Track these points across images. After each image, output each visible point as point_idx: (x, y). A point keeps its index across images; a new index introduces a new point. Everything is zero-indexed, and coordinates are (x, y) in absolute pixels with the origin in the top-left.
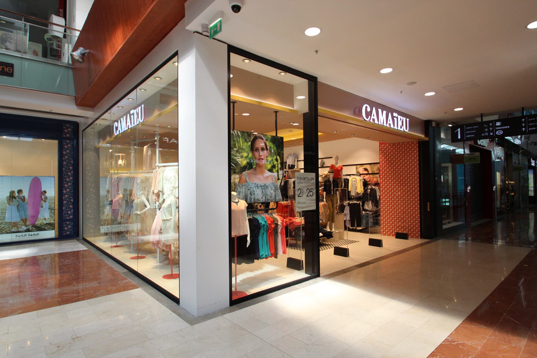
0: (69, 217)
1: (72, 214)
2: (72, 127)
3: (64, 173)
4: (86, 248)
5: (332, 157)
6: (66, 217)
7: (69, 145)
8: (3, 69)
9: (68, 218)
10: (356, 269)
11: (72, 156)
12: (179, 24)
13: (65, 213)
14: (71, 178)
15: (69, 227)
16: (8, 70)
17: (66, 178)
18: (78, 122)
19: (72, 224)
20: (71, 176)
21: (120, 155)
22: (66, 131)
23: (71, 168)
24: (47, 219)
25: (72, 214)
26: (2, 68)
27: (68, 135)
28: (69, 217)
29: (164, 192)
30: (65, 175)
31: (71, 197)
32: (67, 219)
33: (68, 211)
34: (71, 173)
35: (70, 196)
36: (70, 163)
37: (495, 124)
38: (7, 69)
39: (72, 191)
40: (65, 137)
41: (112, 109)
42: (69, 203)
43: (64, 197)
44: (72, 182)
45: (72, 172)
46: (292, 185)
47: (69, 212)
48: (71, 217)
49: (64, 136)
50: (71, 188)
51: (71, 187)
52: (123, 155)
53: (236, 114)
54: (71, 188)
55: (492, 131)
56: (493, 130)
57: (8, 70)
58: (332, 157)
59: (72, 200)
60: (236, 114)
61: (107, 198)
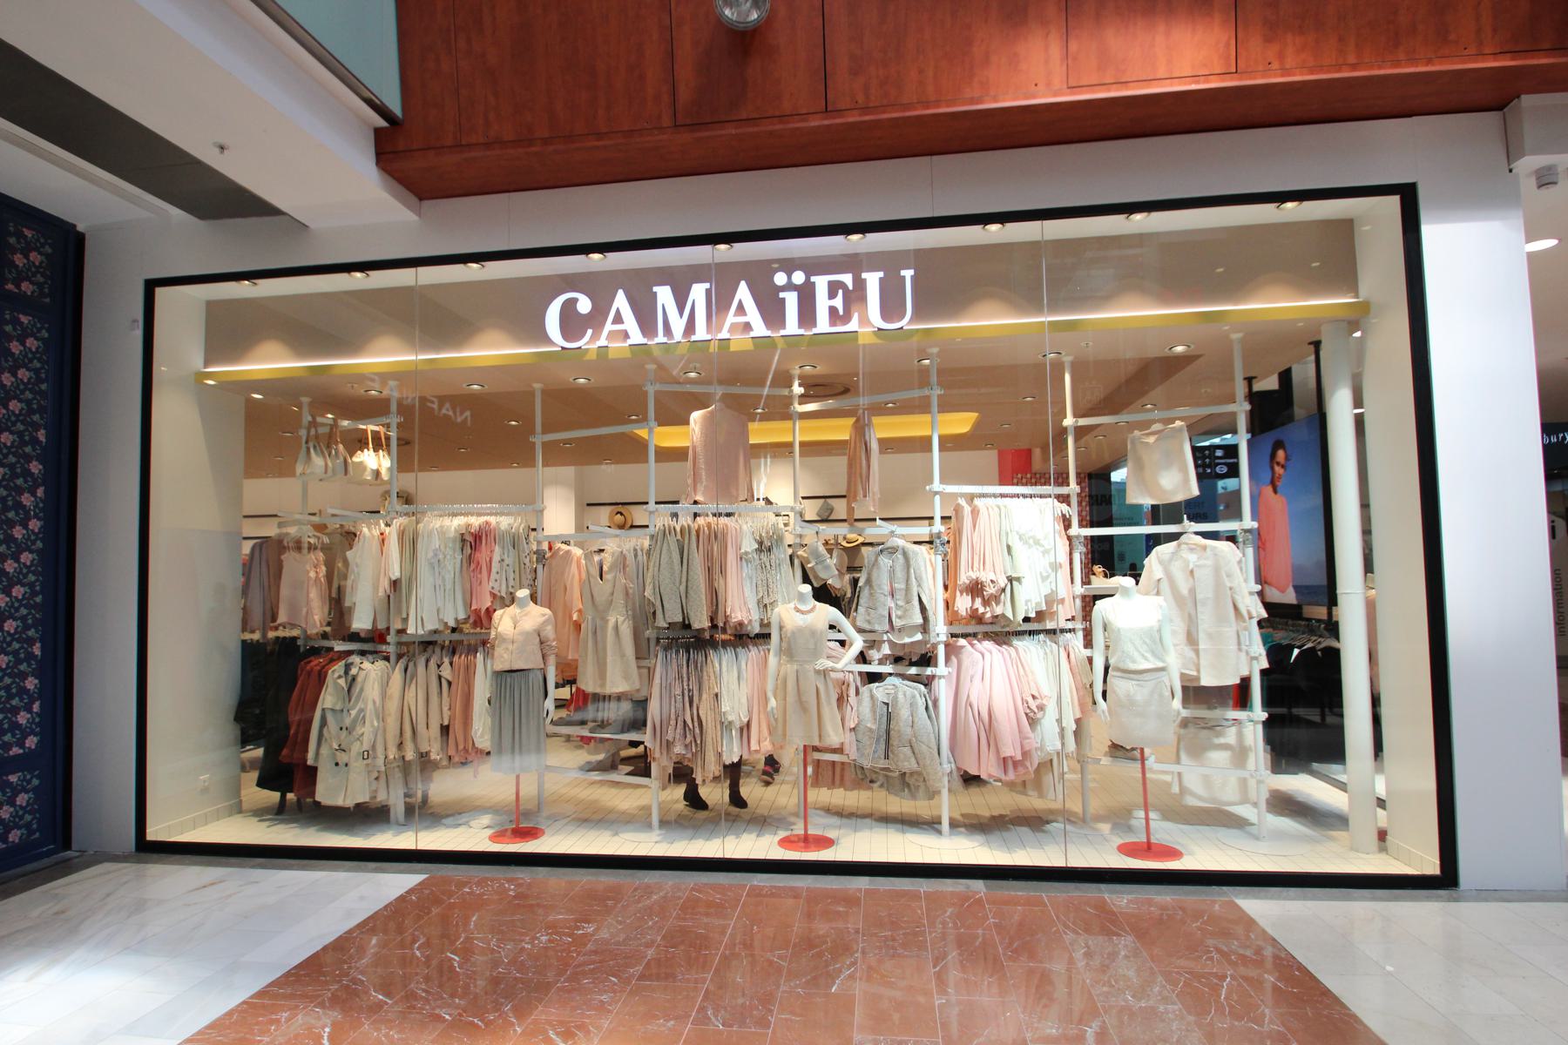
0: (21, 744)
1: (38, 725)
2: (48, 250)
4: (423, 877)
5: (588, 507)
7: (31, 343)
9: (15, 750)
10: (908, 799)
12: (1414, 117)
14: (35, 525)
15: (22, 799)
18: (80, 228)
19: (36, 782)
20: (36, 516)
21: (1234, 432)
22: (19, 260)
24: (1244, 651)
25: (38, 725)
27: (27, 287)
28: (21, 744)
29: (347, 604)
32: (9, 757)
34: (33, 494)
35: (27, 628)
37: (1214, 452)
39: (39, 599)
40: (10, 291)
42: (23, 667)
44: (39, 544)
45: (40, 492)
46: (457, 588)
47: (23, 718)
49: (10, 286)
50: (32, 578)
51: (34, 573)
52: (378, 432)
54: (32, 578)
55: (1209, 466)
56: (1210, 463)
58: (588, 505)
59: (37, 650)
61: (404, 616)
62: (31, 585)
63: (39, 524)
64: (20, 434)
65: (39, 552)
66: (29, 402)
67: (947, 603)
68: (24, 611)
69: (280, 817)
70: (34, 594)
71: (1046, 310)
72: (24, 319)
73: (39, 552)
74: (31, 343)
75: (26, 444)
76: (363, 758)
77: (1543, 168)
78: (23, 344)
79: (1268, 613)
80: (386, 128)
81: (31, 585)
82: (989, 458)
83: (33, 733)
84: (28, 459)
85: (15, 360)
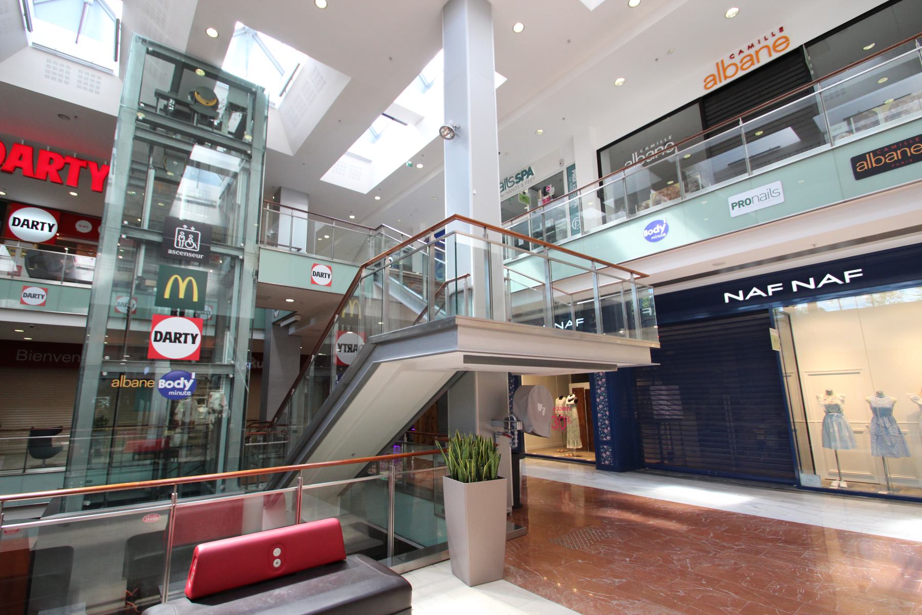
3: (600, 429)
5: (406, 123)
6: (603, 437)
7: (601, 398)
8: (904, 153)
9: (604, 439)
11: (607, 404)
13: (600, 431)
14: (604, 380)
16: (914, 151)
17: (598, 381)
23: (607, 422)
26: (901, 153)
27: (607, 462)
30: (601, 434)
31: (605, 408)
33: (604, 429)
34: (607, 429)
35: (604, 407)
36: (606, 415)
38: (912, 150)
39: (606, 400)
41: (857, 113)
42: (604, 417)
43: (598, 408)
44: (605, 385)
45: (609, 428)
48: (608, 438)
49: (603, 463)
50: (604, 394)
53: (24, 445)
54: (604, 394)
57: (914, 151)
60: (24, 445)
62: (604, 396)
63: (609, 437)
64: (602, 414)
65: (605, 387)
66: (603, 405)
67: (356, 256)
68: (603, 403)
69: (255, 272)
70: (605, 398)
71: (597, 306)
72: (605, 447)
73: (605, 387)
74: (608, 453)
75: (603, 425)
76: (77, 188)
77: (895, 420)
78: (606, 454)
79: (769, 330)
80: (444, 50)
81: (604, 396)
82: (231, 183)
83: (603, 378)
84: (605, 420)
85: (604, 458)
